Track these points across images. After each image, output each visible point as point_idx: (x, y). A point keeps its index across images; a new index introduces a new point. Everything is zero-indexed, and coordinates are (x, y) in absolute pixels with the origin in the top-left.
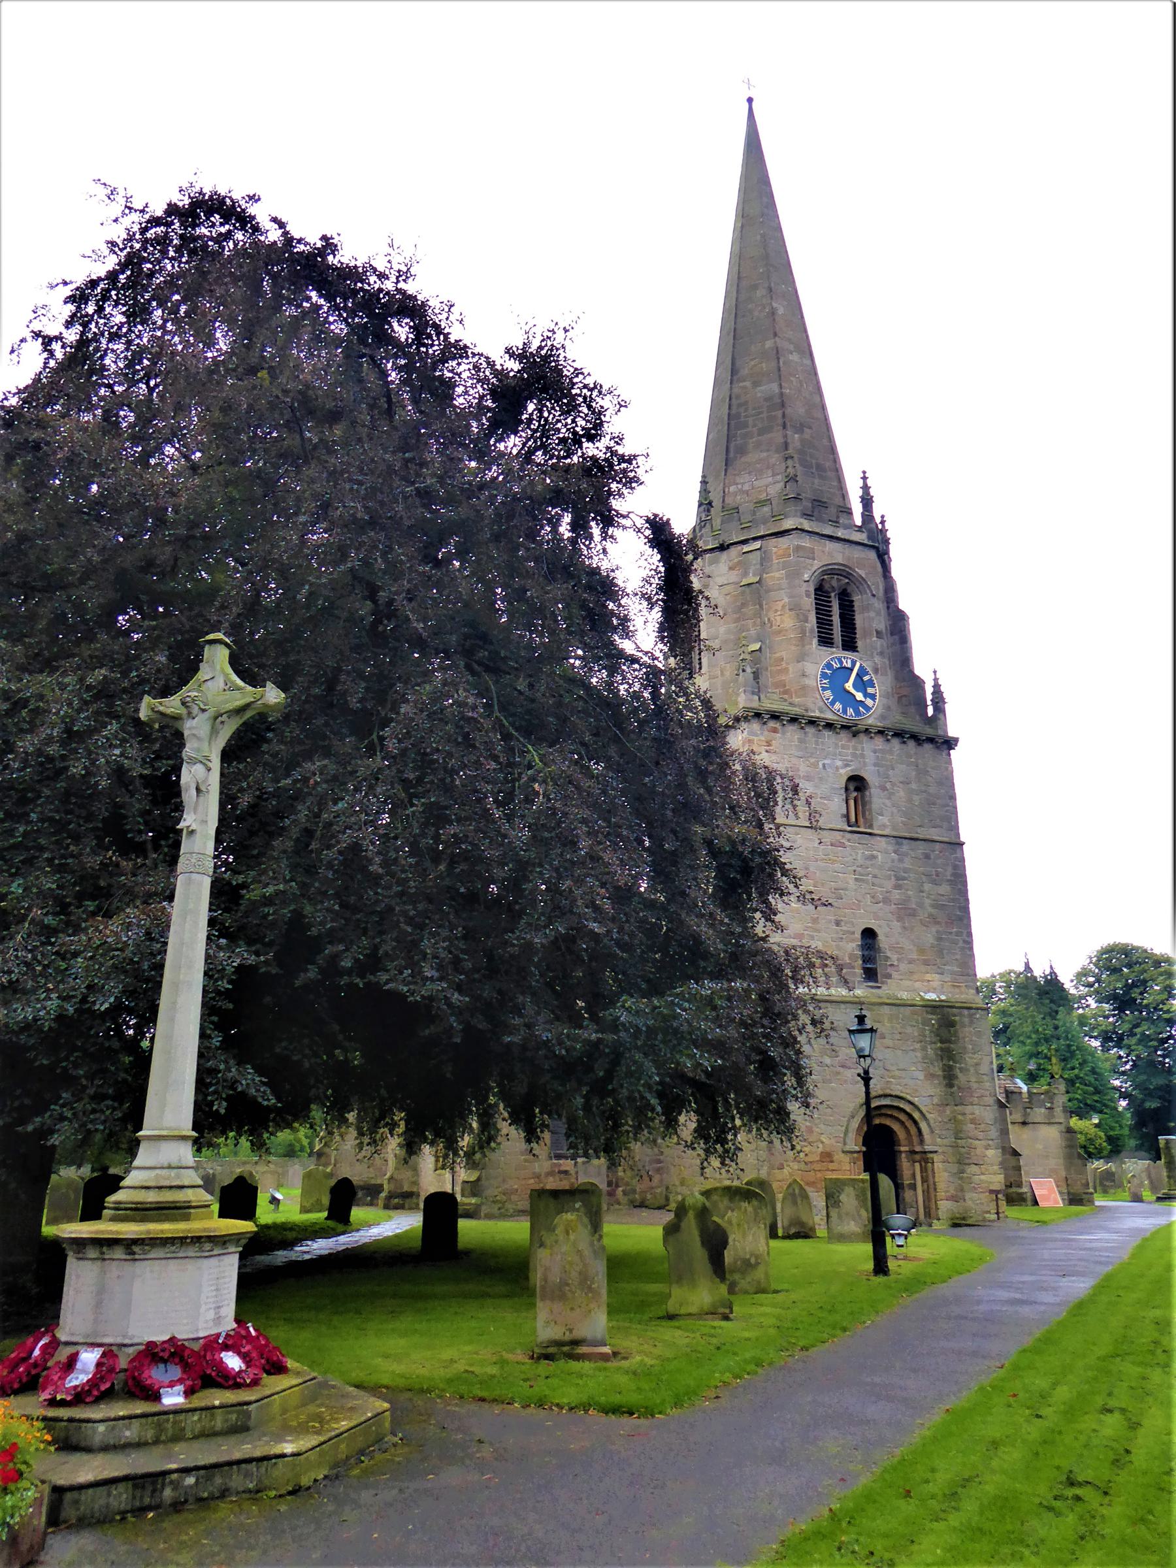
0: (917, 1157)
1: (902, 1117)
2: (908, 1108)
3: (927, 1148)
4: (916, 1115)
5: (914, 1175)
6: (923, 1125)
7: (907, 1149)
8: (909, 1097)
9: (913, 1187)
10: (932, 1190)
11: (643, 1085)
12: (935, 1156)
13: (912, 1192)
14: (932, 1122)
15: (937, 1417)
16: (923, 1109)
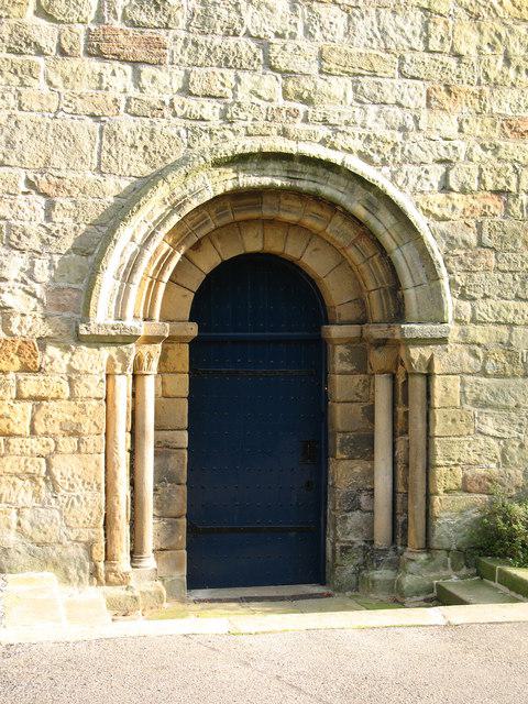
1: (337, 230)
7: (351, 331)
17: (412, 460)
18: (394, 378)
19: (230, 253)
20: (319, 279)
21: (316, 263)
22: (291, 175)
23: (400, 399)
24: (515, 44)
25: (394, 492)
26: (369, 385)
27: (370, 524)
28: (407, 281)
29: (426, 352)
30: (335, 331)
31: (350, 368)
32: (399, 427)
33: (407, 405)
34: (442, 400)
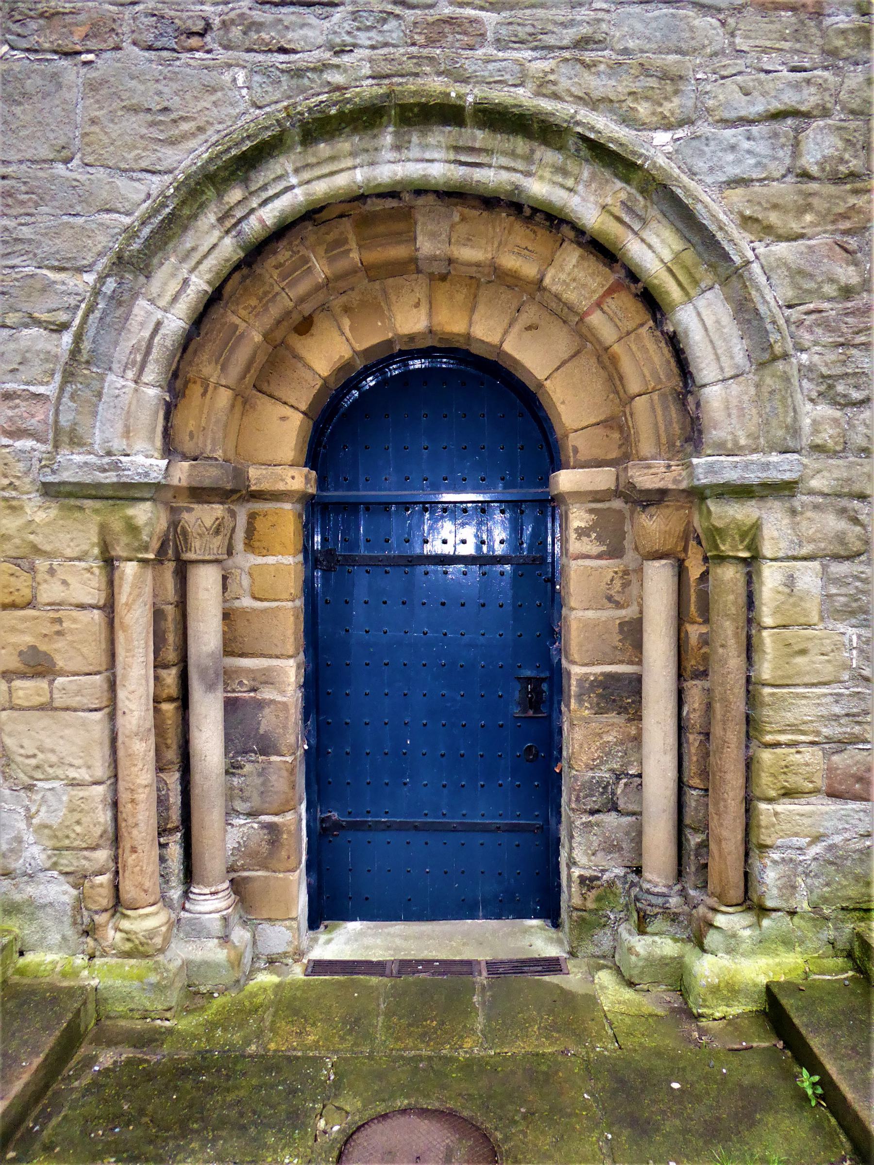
0: (654, 526)
1: (571, 275)
2: (589, 202)
3: (709, 468)
4: (654, 250)
5: (633, 633)
6: (704, 320)
7: (602, 479)
8: (604, 125)
9: (622, 695)
10: (730, 735)
11: (368, 1037)
12: (776, 527)
13: (613, 728)
14: (771, 296)
15: (19, 444)
16: (715, 208)
17: (717, 730)
18: (681, 572)
19: (371, 338)
20: (759, 826)
21: (535, 356)
22: (463, 158)
23: (693, 608)
24: (85, 858)
25: (681, 786)
26: (631, 578)
27: (637, 836)
28: (706, 369)
29: (741, 513)
30: (566, 480)
31: (596, 549)
32: (691, 663)
33: (707, 621)
34: (777, 610)
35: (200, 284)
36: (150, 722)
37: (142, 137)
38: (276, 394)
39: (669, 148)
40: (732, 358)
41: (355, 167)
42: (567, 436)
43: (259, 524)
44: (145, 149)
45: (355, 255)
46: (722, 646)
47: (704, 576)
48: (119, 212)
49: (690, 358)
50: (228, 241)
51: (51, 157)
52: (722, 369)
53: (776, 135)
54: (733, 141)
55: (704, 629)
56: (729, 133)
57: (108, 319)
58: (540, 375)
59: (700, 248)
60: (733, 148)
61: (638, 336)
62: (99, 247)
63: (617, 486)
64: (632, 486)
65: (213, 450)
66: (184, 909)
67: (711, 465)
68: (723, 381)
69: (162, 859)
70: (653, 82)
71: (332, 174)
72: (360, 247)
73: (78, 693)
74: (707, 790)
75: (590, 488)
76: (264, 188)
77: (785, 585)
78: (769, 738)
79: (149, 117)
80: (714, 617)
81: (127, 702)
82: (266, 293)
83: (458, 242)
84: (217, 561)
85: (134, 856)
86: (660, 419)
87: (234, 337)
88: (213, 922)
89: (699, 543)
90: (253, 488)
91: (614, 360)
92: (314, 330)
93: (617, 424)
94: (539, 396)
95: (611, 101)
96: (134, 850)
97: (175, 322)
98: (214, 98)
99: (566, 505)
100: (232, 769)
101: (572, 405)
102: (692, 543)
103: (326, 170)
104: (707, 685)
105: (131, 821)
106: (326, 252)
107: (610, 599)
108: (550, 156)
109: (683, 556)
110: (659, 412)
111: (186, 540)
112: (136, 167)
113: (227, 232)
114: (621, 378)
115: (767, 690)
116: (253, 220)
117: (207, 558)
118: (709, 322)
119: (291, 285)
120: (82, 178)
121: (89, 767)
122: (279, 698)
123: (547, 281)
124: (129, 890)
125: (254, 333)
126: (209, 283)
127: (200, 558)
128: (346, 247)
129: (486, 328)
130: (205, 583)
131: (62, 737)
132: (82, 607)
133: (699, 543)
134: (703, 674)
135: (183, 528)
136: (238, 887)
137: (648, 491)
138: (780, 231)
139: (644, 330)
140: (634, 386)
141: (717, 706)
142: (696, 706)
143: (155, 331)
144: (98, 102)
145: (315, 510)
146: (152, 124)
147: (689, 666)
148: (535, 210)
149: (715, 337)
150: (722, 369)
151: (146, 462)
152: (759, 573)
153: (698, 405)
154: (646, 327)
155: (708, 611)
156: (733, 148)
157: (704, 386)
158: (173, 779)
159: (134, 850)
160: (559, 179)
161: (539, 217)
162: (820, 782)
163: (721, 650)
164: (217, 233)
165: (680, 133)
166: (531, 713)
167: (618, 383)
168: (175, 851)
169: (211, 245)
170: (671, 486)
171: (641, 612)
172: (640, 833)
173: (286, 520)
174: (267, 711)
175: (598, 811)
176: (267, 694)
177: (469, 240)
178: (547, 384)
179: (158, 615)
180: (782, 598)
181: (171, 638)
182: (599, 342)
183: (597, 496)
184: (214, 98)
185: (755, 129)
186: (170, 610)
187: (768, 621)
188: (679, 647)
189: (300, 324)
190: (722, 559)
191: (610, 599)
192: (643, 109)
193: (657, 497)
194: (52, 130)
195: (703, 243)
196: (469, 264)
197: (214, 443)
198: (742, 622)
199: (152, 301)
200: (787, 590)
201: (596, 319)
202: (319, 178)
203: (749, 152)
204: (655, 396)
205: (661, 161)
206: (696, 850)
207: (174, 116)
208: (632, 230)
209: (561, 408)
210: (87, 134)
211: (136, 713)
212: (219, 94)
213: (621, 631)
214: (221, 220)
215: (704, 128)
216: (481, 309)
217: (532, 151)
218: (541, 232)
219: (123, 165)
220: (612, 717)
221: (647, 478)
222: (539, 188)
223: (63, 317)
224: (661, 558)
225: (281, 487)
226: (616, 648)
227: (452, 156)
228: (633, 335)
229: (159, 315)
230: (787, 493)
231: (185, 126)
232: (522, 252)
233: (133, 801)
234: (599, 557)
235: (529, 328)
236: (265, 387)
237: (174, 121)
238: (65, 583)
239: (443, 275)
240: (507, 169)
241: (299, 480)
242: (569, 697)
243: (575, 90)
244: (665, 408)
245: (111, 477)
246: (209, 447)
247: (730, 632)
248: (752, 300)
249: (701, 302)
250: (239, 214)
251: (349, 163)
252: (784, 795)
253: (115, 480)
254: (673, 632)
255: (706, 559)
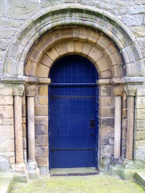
0: (117, 90)
1: (102, 42)
5: (113, 111)
7: (107, 81)
10: (131, 130)
18: (122, 98)
22: (83, 19)
25: (121, 139)
26: (113, 100)
27: (113, 149)
28: (127, 60)
30: (101, 81)
31: (106, 94)
33: (127, 108)
35: (32, 42)
36: (21, 128)
37: (20, 13)
38: (44, 64)
39: (121, 19)
40: (132, 59)
41: (62, 20)
42: (100, 73)
43: (41, 89)
44: (21, 15)
45: (61, 37)
46: (130, 112)
47: (126, 99)
48: (15, 27)
49: (124, 58)
50: (37, 34)
51: (1, 16)
52: (130, 61)
53: (140, 17)
54: (132, 18)
55: (126, 109)
56: (131, 16)
57: (14, 49)
58: (96, 61)
59: (126, 38)
60: (132, 19)
61: (115, 54)
62: (12, 34)
63: (110, 82)
64: (113, 82)
65: (33, 75)
66: (27, 164)
67: (128, 78)
68: (130, 63)
69: (24, 155)
70: (118, 6)
71: (57, 21)
72: (61, 35)
73: (8, 122)
74: (126, 139)
75: (105, 83)
76: (44, 23)
77: (141, 101)
78: (138, 129)
79: (21, 9)
80: (128, 107)
81: (17, 124)
82: (43, 44)
83: (81, 34)
84: (33, 96)
85: (19, 153)
86: (119, 70)
87: (37, 52)
88: (33, 167)
89: (126, 93)
90: (40, 82)
91: (110, 59)
92: (51, 51)
93: (110, 70)
94: (95, 65)
95: (110, 9)
96: (19, 152)
97: (27, 50)
98: (34, 5)
99: (100, 86)
100: (36, 137)
101: (101, 67)
102: (124, 93)
103: (57, 20)
104: (126, 120)
105: (18, 146)
106: (55, 36)
107: (108, 104)
108: (99, 19)
109: (122, 96)
110: (118, 68)
111: (28, 92)
112: (18, 18)
113: (37, 32)
114: (111, 62)
115: (137, 120)
116: (42, 29)
117: (32, 96)
118: (128, 52)
119: (48, 42)
120: (8, 20)
121: (10, 136)
122: (45, 124)
123: (97, 43)
124: (18, 159)
125: (41, 52)
126: (33, 41)
127: (30, 96)
128: (59, 35)
129: (85, 51)
130: (31, 101)
131: (5, 130)
132: (9, 105)
133: (126, 93)
134: (126, 118)
135: (27, 90)
136: (37, 160)
137: (116, 83)
138: (141, 35)
139: (115, 53)
140: (114, 64)
141: (128, 123)
142: (124, 124)
143: (23, 51)
144: (11, 5)
145: (51, 87)
146: (21, 10)
147: (124, 116)
148: (96, 29)
149: (129, 55)
150: (130, 61)
151: (21, 77)
152: (137, 99)
153: (126, 67)
154: (116, 52)
155: (127, 106)
156: (132, 19)
157: (127, 64)
158: (25, 139)
159: (19, 152)
160: (100, 23)
161: (96, 31)
162: (137, 75)
163: (129, 113)
164: (35, 32)
165: (123, 16)
166: (92, 127)
167: (110, 63)
168: (25, 153)
169: (33, 35)
170: (121, 82)
171: (114, 107)
172: (113, 149)
173: (45, 90)
174: (42, 126)
175: (106, 145)
176: (42, 123)
177: (83, 34)
178: (97, 63)
179: (23, 107)
180: (140, 103)
181: (25, 111)
182: (107, 55)
183: (106, 84)
184: (34, 5)
185: (136, 16)
186: (25, 106)
187: (138, 107)
188: (121, 113)
189: (49, 50)
190: (130, 96)
191: (108, 104)
192: (116, 11)
193: (118, 84)
194: (2, 11)
195: (127, 37)
196: (82, 39)
197: (33, 73)
198: (133, 108)
199: (22, 45)
200: (141, 102)
201: (107, 50)
202: (55, 22)
203: (135, 20)
204: (118, 65)
205: (119, 21)
206: (124, 151)
207: (26, 9)
208: (114, 34)
209: (100, 67)
210: (9, 12)
211: (19, 126)
212: (35, 5)
213: (111, 110)
214: (36, 29)
215: (127, 16)
216: (84, 48)
217: (96, 18)
218: (96, 33)
219: (16, 18)
220: (109, 127)
221: (116, 81)
222: (97, 25)
223: (5, 48)
224: (119, 96)
225: (45, 82)
226: (109, 114)
227: (80, 18)
228: (113, 54)
229: (24, 48)
230: (142, 84)
231: (28, 11)
232: (94, 37)
233: (19, 143)
234: (107, 96)
235: (93, 52)
236: (42, 62)
237: (26, 10)
238: (5, 100)
239: (76, 40)
240: (91, 21)
241: (49, 81)
242: (101, 123)
243: (104, 7)
244: (120, 68)
245: (15, 79)
246: (32, 74)
247: (131, 110)
248: (136, 48)
249: (126, 48)
250: (39, 28)
251: (61, 19)
252: (140, 139)
253: (16, 80)
254: (120, 110)
255: (127, 96)
